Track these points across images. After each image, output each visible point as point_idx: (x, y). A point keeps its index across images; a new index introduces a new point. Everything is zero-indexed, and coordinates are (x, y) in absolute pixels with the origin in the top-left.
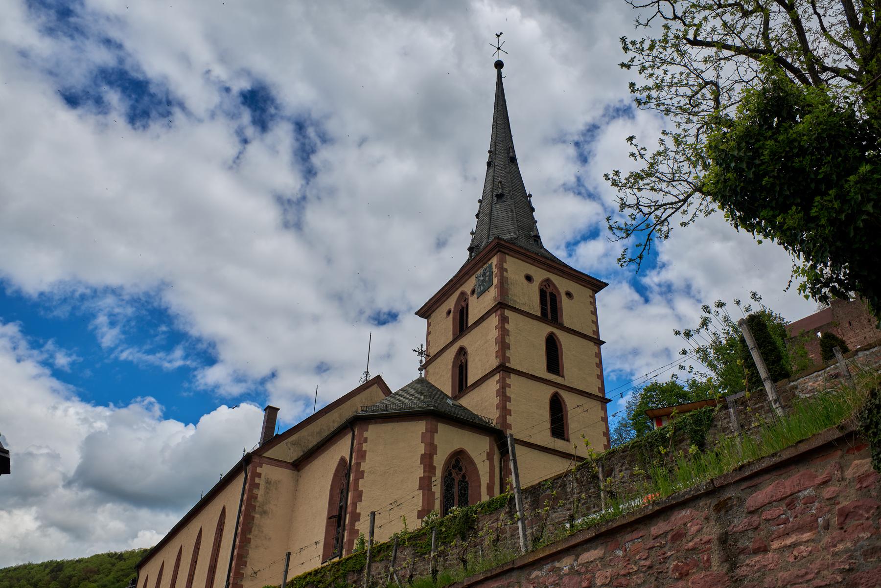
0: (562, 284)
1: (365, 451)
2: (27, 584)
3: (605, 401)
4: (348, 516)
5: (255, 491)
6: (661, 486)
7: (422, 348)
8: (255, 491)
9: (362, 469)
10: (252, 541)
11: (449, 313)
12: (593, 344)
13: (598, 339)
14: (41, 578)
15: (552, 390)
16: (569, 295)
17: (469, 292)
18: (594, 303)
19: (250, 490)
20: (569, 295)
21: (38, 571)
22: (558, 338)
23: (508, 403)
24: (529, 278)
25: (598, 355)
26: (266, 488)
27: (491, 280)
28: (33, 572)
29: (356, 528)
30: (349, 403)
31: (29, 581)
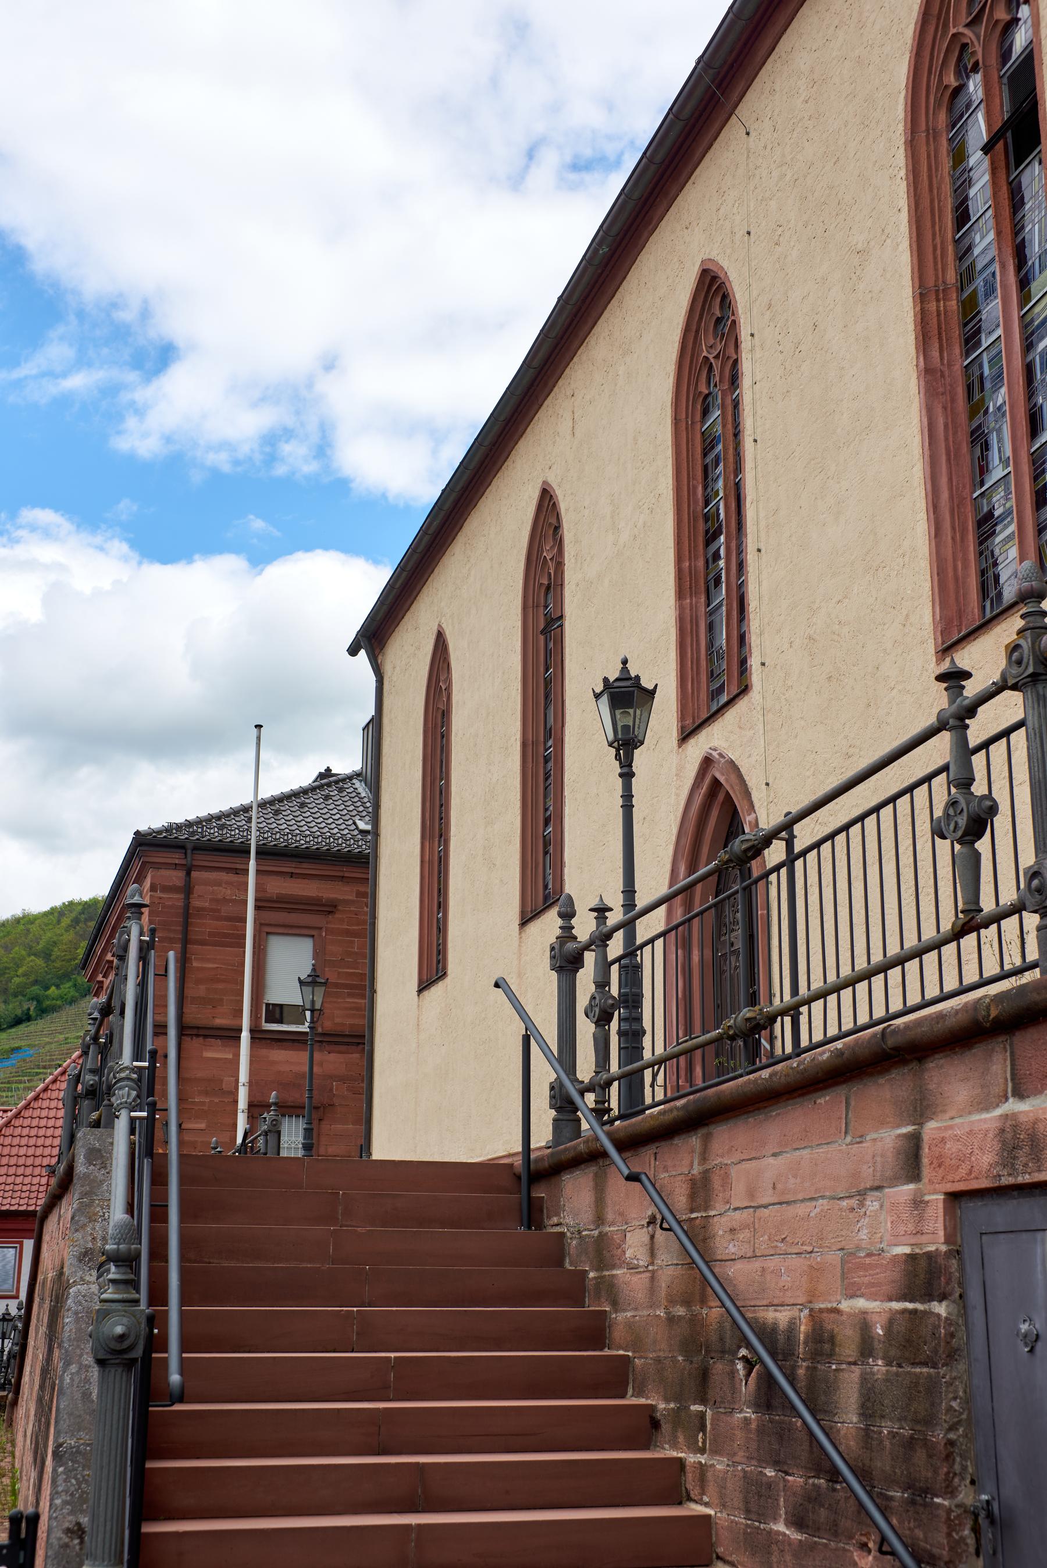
2: (29, 956)
6: (722, 552)
14: (55, 939)
21: (46, 925)
28: (34, 928)
31: (31, 948)
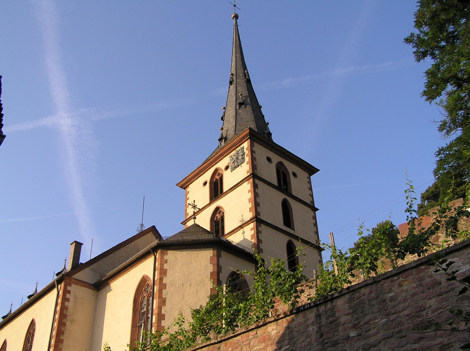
0: (291, 167)
1: (166, 270)
3: (320, 250)
4: (154, 317)
5: (66, 303)
7: (194, 203)
8: (66, 303)
9: (164, 282)
10: (64, 341)
11: (205, 184)
12: (311, 210)
13: (314, 206)
15: (287, 239)
16: (294, 175)
17: (223, 168)
18: (310, 182)
19: (63, 303)
20: (294, 175)
22: (290, 204)
23: (260, 244)
24: (269, 160)
25: (315, 218)
26: (75, 302)
27: (243, 158)
29: (162, 325)
30: (133, 243)
